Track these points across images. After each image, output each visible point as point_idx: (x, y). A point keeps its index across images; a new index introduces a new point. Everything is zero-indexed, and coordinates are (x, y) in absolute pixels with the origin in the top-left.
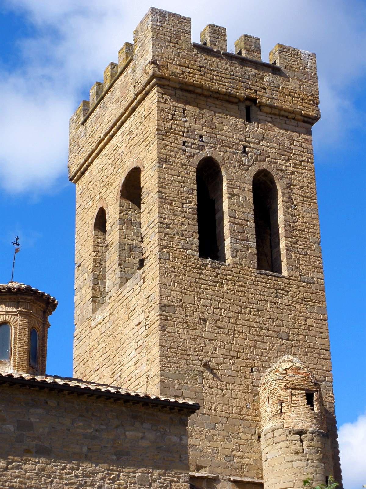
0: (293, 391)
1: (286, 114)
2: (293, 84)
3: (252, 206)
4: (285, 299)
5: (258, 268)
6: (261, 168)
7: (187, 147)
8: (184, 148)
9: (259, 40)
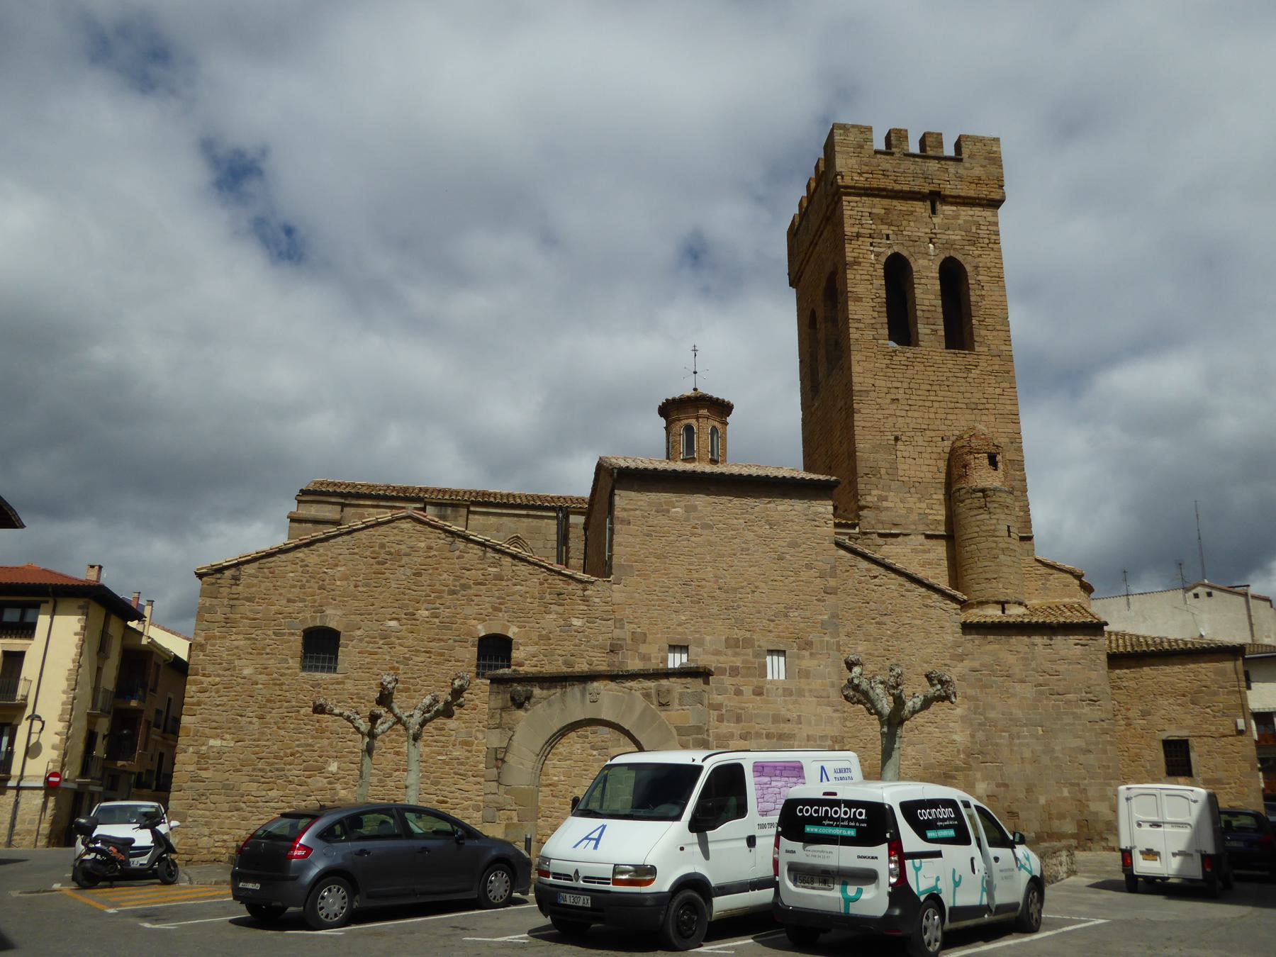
0: (976, 455)
1: (971, 201)
2: (978, 171)
3: (939, 293)
4: (975, 373)
5: (947, 348)
6: (948, 256)
7: (874, 247)
8: (872, 248)
9: (941, 134)
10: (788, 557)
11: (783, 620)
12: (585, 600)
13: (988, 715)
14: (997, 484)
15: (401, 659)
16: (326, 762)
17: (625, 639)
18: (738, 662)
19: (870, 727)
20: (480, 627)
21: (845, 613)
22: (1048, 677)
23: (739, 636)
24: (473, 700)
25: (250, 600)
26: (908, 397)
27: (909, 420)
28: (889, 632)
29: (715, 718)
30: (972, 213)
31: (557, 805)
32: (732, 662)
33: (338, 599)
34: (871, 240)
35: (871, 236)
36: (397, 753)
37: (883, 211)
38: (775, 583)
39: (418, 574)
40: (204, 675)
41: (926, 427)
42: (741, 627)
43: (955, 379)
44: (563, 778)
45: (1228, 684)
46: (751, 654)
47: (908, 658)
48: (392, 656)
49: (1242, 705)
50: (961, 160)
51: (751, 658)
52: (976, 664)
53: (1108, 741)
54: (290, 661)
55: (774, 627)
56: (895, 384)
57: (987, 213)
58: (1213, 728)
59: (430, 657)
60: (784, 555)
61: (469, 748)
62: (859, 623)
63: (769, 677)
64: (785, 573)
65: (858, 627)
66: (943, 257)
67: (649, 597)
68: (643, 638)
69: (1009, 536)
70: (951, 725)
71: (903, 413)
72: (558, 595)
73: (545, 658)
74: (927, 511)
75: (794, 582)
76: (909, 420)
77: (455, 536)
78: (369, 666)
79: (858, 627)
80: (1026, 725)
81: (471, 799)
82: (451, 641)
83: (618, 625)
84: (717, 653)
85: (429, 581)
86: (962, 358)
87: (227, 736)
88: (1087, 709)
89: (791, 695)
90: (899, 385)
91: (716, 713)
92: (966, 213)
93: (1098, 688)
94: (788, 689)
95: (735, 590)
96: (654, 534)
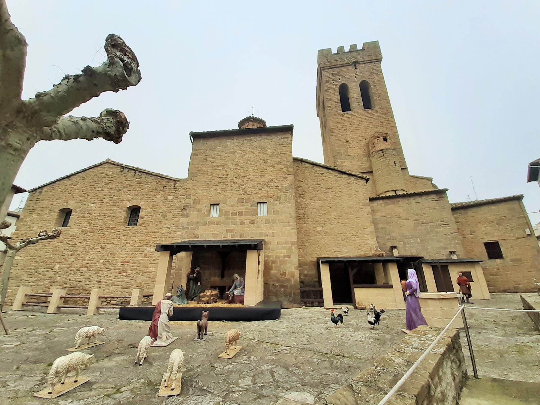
0: (378, 139)
1: (369, 61)
10: (269, 161)
11: (266, 189)
12: (175, 188)
13: (391, 235)
14: (388, 147)
15: (94, 219)
16: (55, 265)
17: (190, 203)
18: (243, 209)
19: (323, 239)
20: (128, 203)
21: (309, 190)
22: (420, 216)
23: (244, 198)
24: (119, 235)
25: (43, 200)
26: (350, 127)
27: (351, 135)
28: (331, 196)
29: (230, 236)
30: (370, 65)
31: (150, 282)
32: (240, 209)
33: (75, 197)
34: (333, 81)
35: (333, 80)
36: (84, 260)
37: (337, 72)
38: (262, 173)
39: (107, 184)
40: (20, 231)
41: (358, 136)
42: (245, 194)
43: (369, 119)
44: (154, 269)
45: (517, 214)
46: (249, 205)
47: (341, 206)
48: (90, 218)
49: (527, 223)
50: (364, 49)
51: (249, 207)
52: (384, 214)
53: (457, 243)
54: (51, 223)
55: (261, 192)
56: (345, 124)
57: (376, 64)
58: (512, 235)
59: (105, 217)
60: (268, 160)
61: (114, 256)
62: (316, 194)
63: (259, 215)
64: (267, 168)
65: (316, 195)
66: (360, 81)
67: (203, 184)
68: (198, 202)
69: (395, 165)
70: (365, 236)
71: (349, 133)
72: (164, 187)
73: (154, 214)
74: (361, 164)
75: (272, 171)
76: (351, 135)
77: (124, 168)
78: (80, 223)
79: (316, 195)
80: (411, 238)
81: (111, 280)
82: (115, 210)
83: (188, 197)
84: (232, 206)
85: (111, 187)
86: (370, 111)
87: (22, 255)
88: (442, 229)
89: (269, 222)
90: (347, 124)
91: (231, 234)
92: (368, 66)
93: (447, 219)
94: (268, 220)
95: (244, 177)
96: (208, 158)
